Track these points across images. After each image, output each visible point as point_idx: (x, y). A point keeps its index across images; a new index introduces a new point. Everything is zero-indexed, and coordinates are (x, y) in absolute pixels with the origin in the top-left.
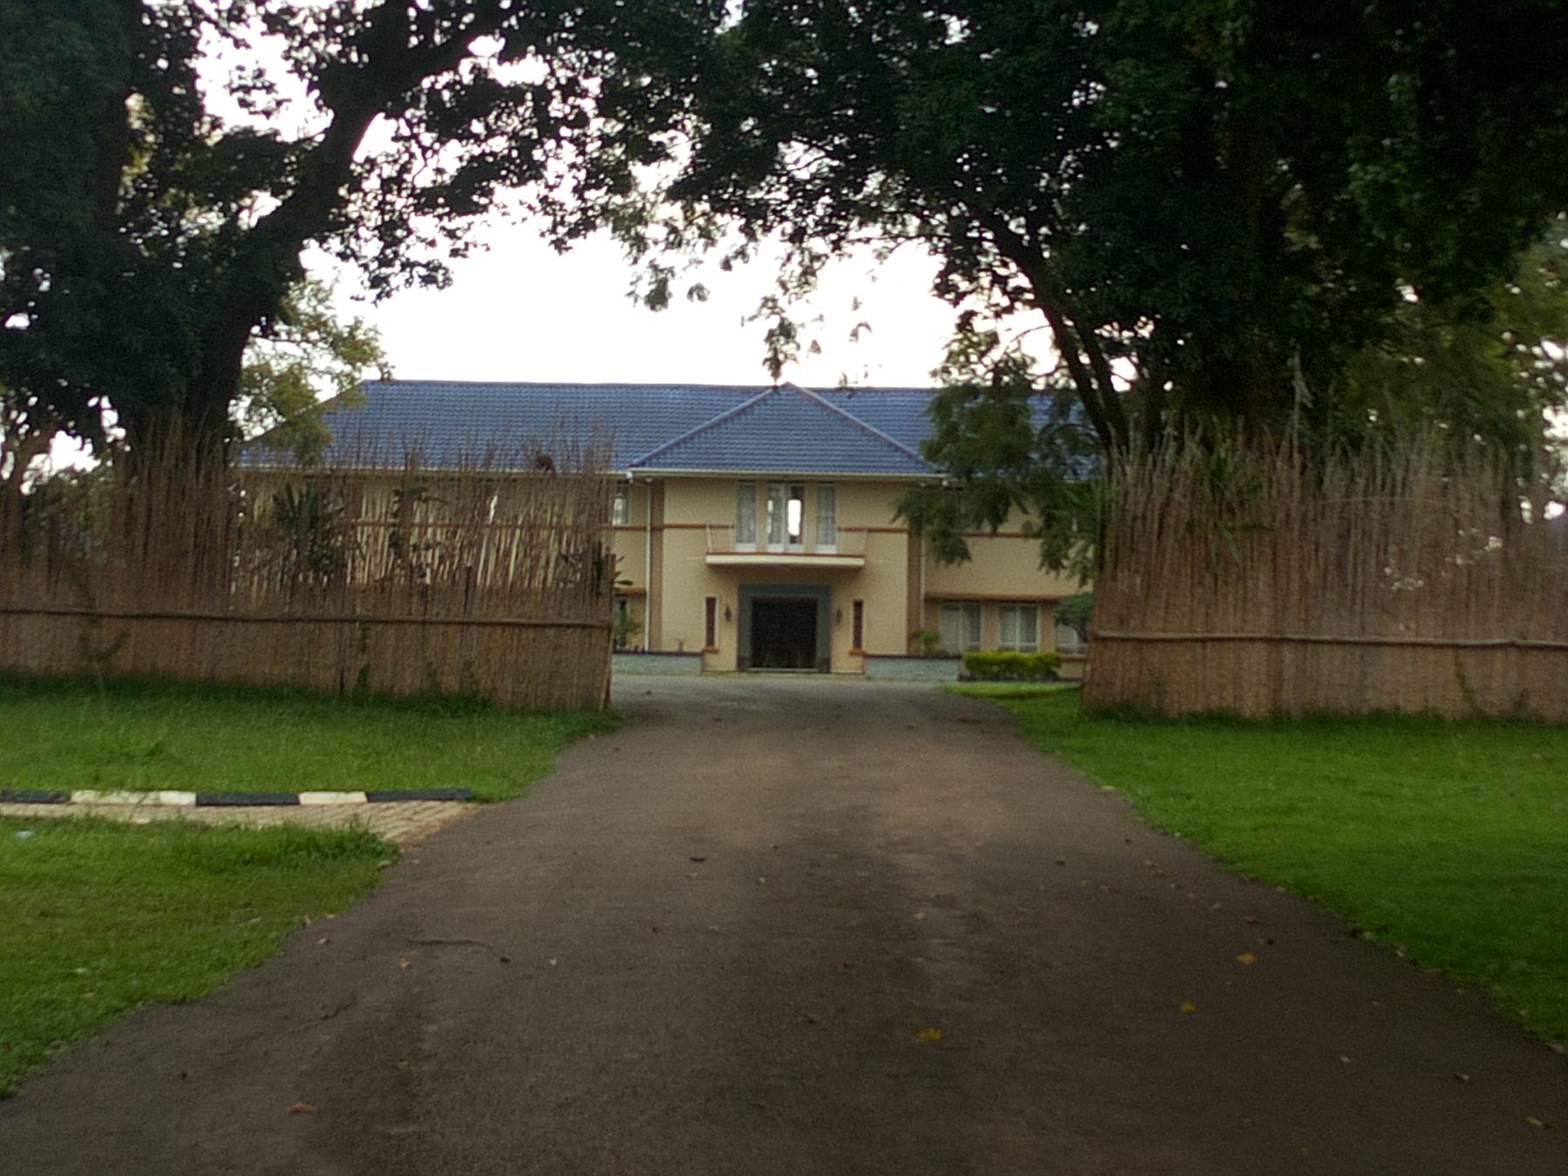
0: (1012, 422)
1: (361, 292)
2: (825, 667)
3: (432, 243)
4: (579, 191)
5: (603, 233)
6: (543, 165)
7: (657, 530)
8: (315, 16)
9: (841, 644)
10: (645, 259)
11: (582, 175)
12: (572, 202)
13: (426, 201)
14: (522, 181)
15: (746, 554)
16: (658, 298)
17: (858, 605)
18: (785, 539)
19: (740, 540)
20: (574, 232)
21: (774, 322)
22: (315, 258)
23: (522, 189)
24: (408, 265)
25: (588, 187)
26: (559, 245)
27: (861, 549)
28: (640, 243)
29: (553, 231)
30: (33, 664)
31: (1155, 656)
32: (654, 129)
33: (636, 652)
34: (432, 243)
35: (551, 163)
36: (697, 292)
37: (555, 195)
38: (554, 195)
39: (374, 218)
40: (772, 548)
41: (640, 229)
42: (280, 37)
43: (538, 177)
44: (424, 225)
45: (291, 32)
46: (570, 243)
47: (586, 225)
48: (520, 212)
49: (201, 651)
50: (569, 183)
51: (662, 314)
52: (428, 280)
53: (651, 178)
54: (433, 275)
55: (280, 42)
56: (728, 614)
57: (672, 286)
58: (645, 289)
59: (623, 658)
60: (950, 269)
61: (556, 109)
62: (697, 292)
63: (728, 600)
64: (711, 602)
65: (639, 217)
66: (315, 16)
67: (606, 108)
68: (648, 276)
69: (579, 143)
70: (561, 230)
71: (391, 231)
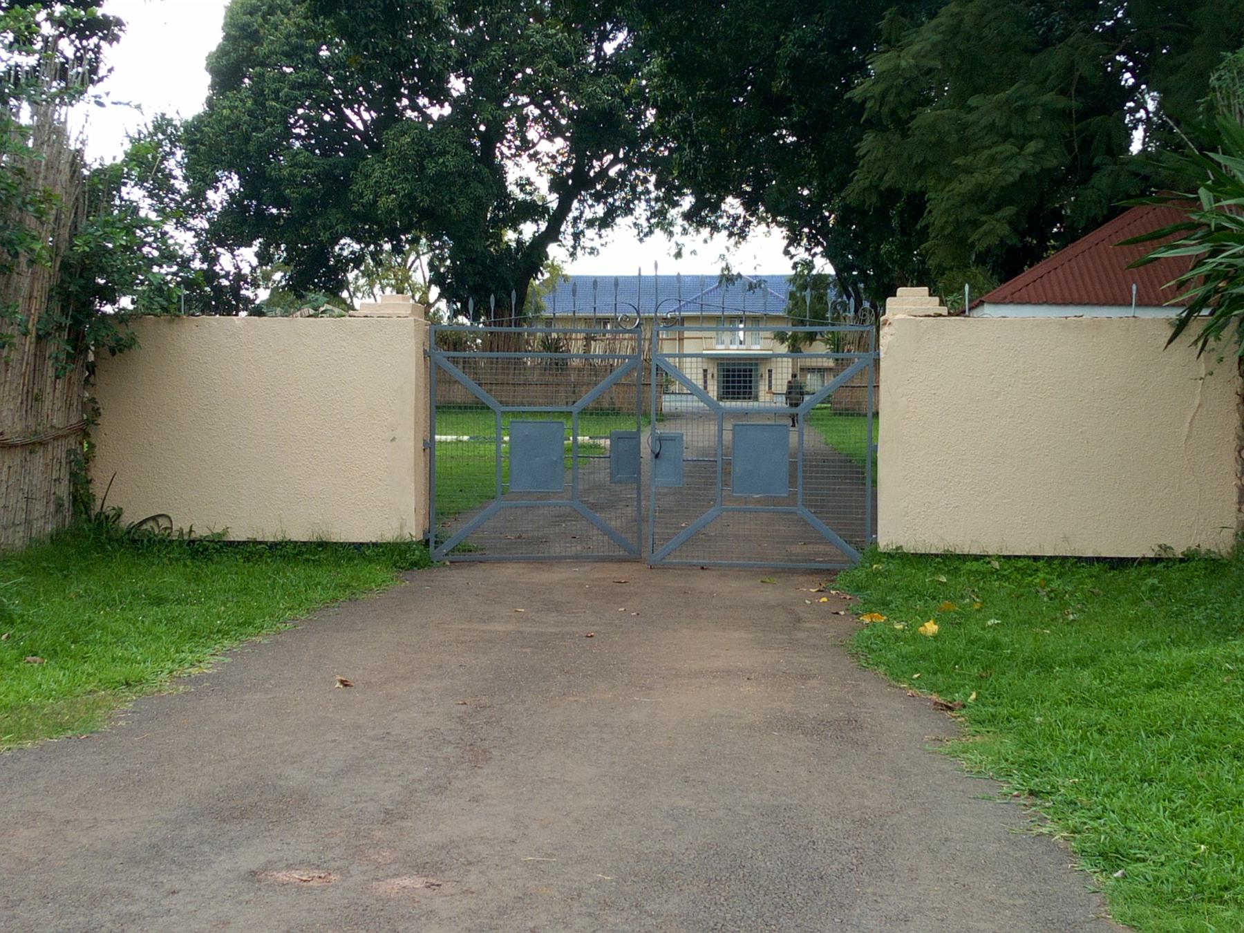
0: (822, 298)
1: (565, 259)
2: (756, 398)
3: (592, 240)
4: (648, 220)
5: (657, 231)
6: (634, 209)
7: (681, 339)
8: (547, 154)
9: (763, 388)
10: (673, 240)
11: (649, 214)
12: (645, 224)
13: (590, 223)
14: (626, 215)
15: (720, 350)
16: (678, 255)
17: (770, 371)
18: (737, 342)
19: (717, 343)
20: (646, 235)
21: (724, 265)
22: (552, 249)
23: (626, 218)
24: (584, 248)
25: (651, 217)
26: (641, 240)
27: (770, 347)
28: (671, 234)
29: (639, 235)
30: (459, 401)
31: (858, 393)
32: (676, 195)
33: (672, 393)
34: (592, 240)
35: (637, 208)
36: (694, 252)
37: (639, 222)
38: (638, 222)
39: (570, 230)
40: (732, 347)
41: (671, 229)
42: (534, 162)
43: (632, 214)
44: (590, 233)
45: (538, 160)
46: (645, 239)
47: (651, 232)
48: (624, 228)
49: (840, 403)
50: (644, 217)
51: (679, 260)
52: (591, 253)
53: (673, 213)
54: (593, 251)
55: (534, 164)
56: (713, 376)
57: (683, 251)
58: (674, 251)
59: (667, 396)
60: (788, 245)
61: (640, 189)
62: (694, 252)
63: (713, 370)
64: (705, 371)
65: (671, 224)
66: (547, 154)
67: (657, 187)
68: (674, 246)
69: (648, 201)
70: (642, 235)
71: (577, 236)
